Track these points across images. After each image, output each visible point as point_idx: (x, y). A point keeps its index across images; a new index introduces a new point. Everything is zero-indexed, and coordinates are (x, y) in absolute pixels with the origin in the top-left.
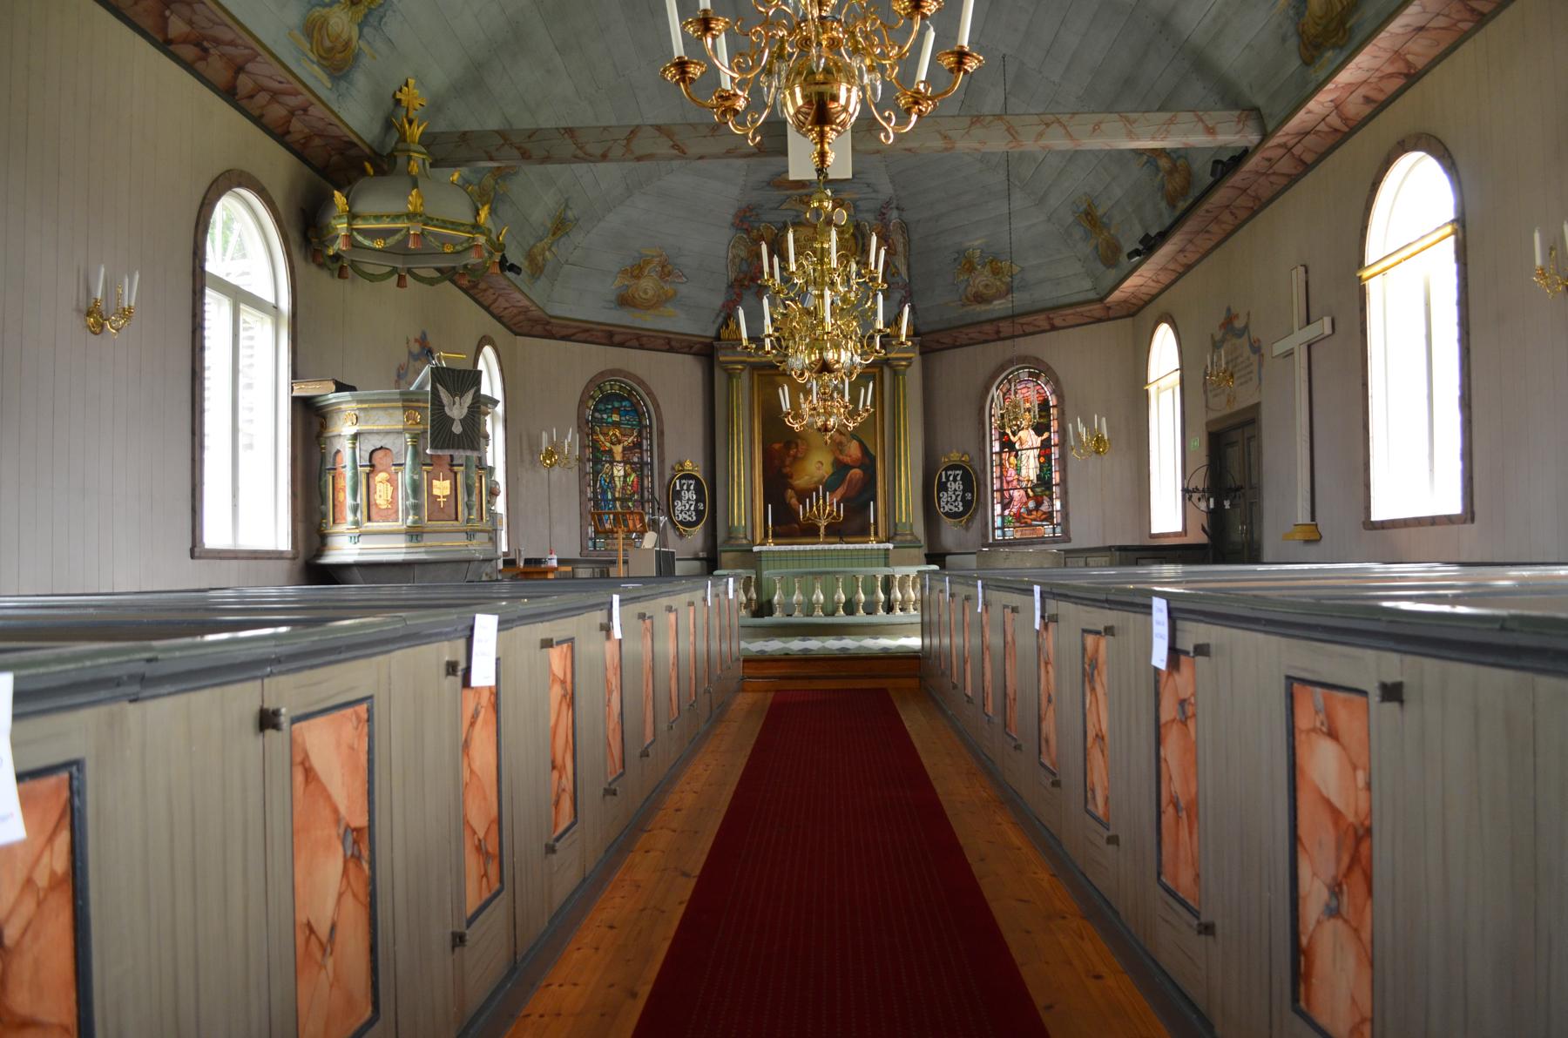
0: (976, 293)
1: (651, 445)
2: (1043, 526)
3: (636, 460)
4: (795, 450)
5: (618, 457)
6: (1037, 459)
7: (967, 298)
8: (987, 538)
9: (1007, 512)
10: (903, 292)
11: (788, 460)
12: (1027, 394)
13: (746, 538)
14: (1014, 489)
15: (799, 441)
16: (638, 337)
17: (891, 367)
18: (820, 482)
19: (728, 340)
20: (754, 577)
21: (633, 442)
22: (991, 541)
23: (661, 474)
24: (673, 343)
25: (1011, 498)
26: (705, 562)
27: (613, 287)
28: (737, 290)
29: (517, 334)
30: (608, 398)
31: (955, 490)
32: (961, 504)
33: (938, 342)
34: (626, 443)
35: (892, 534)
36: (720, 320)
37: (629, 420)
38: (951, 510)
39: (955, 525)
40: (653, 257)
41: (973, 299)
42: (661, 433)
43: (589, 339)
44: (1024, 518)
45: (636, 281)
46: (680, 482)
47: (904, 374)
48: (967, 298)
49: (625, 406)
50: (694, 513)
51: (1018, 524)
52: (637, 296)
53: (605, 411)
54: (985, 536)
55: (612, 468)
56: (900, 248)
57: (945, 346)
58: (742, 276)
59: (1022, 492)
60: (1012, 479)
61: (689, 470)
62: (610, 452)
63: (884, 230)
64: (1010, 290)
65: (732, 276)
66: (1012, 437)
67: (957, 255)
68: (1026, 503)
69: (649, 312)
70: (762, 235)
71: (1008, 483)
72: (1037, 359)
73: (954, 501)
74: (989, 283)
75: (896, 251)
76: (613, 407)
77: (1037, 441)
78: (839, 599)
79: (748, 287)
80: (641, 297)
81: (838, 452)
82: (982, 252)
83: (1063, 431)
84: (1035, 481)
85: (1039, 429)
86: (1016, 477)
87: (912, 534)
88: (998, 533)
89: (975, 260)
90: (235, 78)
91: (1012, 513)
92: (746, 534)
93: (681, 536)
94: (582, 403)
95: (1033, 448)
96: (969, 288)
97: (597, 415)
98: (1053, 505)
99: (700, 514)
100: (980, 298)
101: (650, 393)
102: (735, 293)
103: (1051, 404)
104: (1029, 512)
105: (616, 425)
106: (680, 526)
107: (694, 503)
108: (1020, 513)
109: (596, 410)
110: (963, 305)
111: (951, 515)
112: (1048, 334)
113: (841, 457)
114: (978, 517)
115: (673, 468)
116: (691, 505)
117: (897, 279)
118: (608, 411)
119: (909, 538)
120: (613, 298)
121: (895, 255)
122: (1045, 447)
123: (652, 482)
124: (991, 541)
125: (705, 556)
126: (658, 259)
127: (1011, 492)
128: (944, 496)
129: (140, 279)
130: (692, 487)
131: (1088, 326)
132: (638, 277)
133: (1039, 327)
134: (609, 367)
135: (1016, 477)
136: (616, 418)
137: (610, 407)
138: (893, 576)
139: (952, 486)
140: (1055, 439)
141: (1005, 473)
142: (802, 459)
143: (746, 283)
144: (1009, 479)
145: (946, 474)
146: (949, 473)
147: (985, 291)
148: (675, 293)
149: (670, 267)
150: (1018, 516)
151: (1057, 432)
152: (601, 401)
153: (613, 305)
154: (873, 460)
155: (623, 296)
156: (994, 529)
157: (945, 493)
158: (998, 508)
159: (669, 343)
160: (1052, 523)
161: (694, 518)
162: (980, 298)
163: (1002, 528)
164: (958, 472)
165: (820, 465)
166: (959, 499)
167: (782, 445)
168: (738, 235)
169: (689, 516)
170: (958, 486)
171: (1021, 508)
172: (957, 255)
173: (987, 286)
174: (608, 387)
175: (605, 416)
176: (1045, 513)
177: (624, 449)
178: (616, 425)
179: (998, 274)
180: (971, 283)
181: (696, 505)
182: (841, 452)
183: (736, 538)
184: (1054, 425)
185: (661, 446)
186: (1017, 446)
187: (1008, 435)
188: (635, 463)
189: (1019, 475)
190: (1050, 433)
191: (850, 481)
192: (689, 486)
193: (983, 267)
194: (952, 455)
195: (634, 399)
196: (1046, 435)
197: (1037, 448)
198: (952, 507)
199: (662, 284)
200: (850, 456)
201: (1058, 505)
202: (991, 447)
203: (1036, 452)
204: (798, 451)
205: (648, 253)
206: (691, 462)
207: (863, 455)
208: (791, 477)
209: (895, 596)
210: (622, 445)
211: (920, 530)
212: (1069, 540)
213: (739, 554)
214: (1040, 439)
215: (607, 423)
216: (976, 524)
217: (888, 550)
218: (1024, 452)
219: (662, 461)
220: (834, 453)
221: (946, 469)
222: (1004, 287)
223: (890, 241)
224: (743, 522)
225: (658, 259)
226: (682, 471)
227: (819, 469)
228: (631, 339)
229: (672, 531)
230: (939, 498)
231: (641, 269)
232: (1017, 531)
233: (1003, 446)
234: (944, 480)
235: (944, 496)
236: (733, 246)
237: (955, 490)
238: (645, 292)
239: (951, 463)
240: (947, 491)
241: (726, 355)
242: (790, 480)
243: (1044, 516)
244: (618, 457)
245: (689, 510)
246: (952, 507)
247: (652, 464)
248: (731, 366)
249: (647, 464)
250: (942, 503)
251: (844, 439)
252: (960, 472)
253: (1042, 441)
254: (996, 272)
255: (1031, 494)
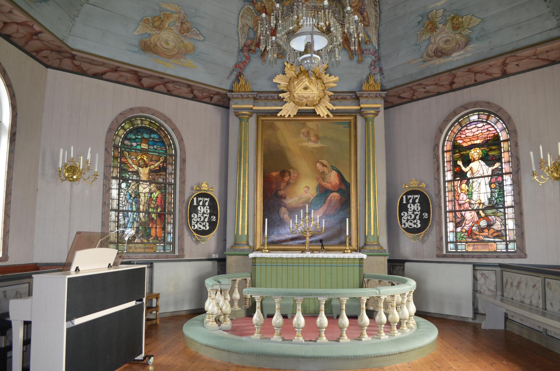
0: (437, 48)
1: (175, 170)
2: (495, 242)
3: (161, 180)
4: (288, 177)
5: (144, 177)
6: (488, 186)
7: (428, 55)
8: (442, 251)
9: (459, 229)
10: (373, 57)
11: (283, 185)
12: (477, 133)
13: (248, 244)
14: (466, 211)
15: (291, 171)
16: (165, 84)
17: (362, 115)
18: (306, 202)
19: (239, 92)
20: (249, 279)
21: (159, 166)
22: (444, 252)
23: (182, 192)
24: (196, 92)
25: (463, 218)
26: (216, 262)
27: (136, 33)
28: (246, 54)
29: (48, 66)
30: (138, 130)
31: (414, 211)
32: (419, 222)
33: (399, 97)
34: (152, 167)
35: (362, 245)
36: (233, 77)
37: (156, 149)
38: (410, 226)
39: (414, 239)
40: (172, 12)
41: (433, 54)
42: (183, 161)
43: (121, 80)
44: (476, 235)
45: (158, 32)
46: (197, 199)
47: (373, 121)
48: (428, 55)
49: (154, 138)
50: (207, 224)
51: (470, 240)
52: (158, 45)
53: (134, 140)
54: (440, 248)
55: (138, 186)
56: (372, 20)
57: (404, 100)
58: (249, 42)
59: (474, 213)
60: (463, 202)
61: (205, 190)
62: (137, 173)
63: (361, 4)
64: (468, 42)
65: (243, 42)
66: (463, 168)
67: (420, 18)
68: (478, 222)
69: (170, 61)
70: (265, 7)
71: (460, 205)
72: (488, 103)
73: (414, 219)
74: (449, 38)
75: (369, 23)
76: (143, 138)
77: (488, 170)
78: (321, 324)
79: (254, 51)
80: (163, 47)
81: (321, 179)
82: (445, 10)
83: (516, 160)
84: (487, 204)
85: (487, 159)
86: (468, 200)
87: (378, 245)
88: (451, 246)
89: (438, 20)
90: (322, 244)
91: (464, 230)
92: (248, 242)
93: (197, 242)
94: (112, 130)
95: (484, 177)
96: (431, 46)
97: (126, 142)
98: (505, 225)
99: (213, 225)
100: (440, 53)
101: (175, 129)
102: (244, 56)
103: (502, 139)
104: (481, 230)
105: (143, 151)
106: (195, 234)
107: (208, 216)
108: (472, 230)
109: (125, 138)
110: (424, 61)
111: (409, 230)
112: (498, 81)
113: (323, 183)
114: (434, 232)
115: (192, 188)
116: (206, 217)
117: (369, 46)
118: (137, 140)
119: (376, 248)
120: (136, 42)
121: (368, 26)
122: (497, 174)
123: (175, 199)
124: (444, 252)
125: (217, 257)
126: (177, 15)
127: (463, 213)
128: (405, 215)
129: (91, 150)
130: (207, 204)
131: (541, 69)
132: (159, 28)
133: (491, 75)
134: (139, 105)
135: (468, 200)
136: (144, 146)
137: (139, 137)
138: (379, 297)
139: (412, 207)
140: (506, 168)
141: (457, 197)
142: (295, 184)
143: (253, 48)
144: (461, 202)
145: (406, 197)
146: (409, 196)
147: (445, 46)
148: (194, 48)
149: (189, 25)
150: (470, 233)
151: (509, 162)
152: (131, 132)
153: (136, 49)
154: (348, 186)
155: (146, 42)
156: (447, 243)
157: (406, 213)
158: (451, 226)
159: (192, 92)
160: (506, 241)
161: (208, 228)
162: (440, 53)
163: (455, 242)
164: (416, 196)
165: (307, 189)
166: (418, 217)
167: (278, 173)
168: (246, 7)
169: (204, 226)
170: (417, 207)
171: (472, 226)
172: (420, 18)
173: (447, 41)
174: (139, 122)
175: (134, 144)
176: (498, 231)
177: (151, 171)
178: (143, 151)
179: (458, 28)
180: (433, 41)
181: (210, 216)
182: (323, 179)
183: (239, 245)
184: (506, 157)
185: (183, 170)
186: (469, 175)
187: (460, 166)
188: (160, 183)
189: (470, 199)
190: (502, 163)
191: (331, 200)
192: (204, 203)
193: (445, 24)
194: (412, 183)
195: (162, 133)
196: (497, 165)
197: (488, 176)
198: (412, 224)
199: (182, 38)
200: (331, 183)
201: (511, 224)
202: (444, 176)
203: (488, 180)
204: (290, 178)
205: (170, 9)
206: (207, 184)
207: (340, 183)
208: (285, 198)
209: (380, 318)
210: (148, 168)
211: (384, 241)
212: (525, 256)
213: (242, 257)
214: (490, 169)
215: (136, 150)
216: (432, 238)
217: (362, 259)
218: (475, 180)
219: (183, 182)
220: (318, 179)
221: (407, 194)
222: (463, 40)
223: (365, 14)
224: (246, 232)
225: (177, 15)
226: (200, 190)
227: (306, 192)
228: (159, 85)
229: (189, 237)
230: (401, 217)
231: (162, 21)
232: (469, 246)
233: (455, 175)
234: (405, 202)
235: (405, 215)
236: (242, 17)
237: (414, 211)
238: (167, 44)
239: (410, 190)
240: (407, 211)
241: (237, 104)
242: (284, 200)
243: (495, 234)
244: (144, 177)
245: (203, 221)
246: (412, 224)
247: (175, 184)
248: (241, 112)
249: (170, 184)
250: (403, 221)
251: (325, 170)
252: (418, 196)
253: (493, 171)
254: (456, 28)
255: (483, 215)
